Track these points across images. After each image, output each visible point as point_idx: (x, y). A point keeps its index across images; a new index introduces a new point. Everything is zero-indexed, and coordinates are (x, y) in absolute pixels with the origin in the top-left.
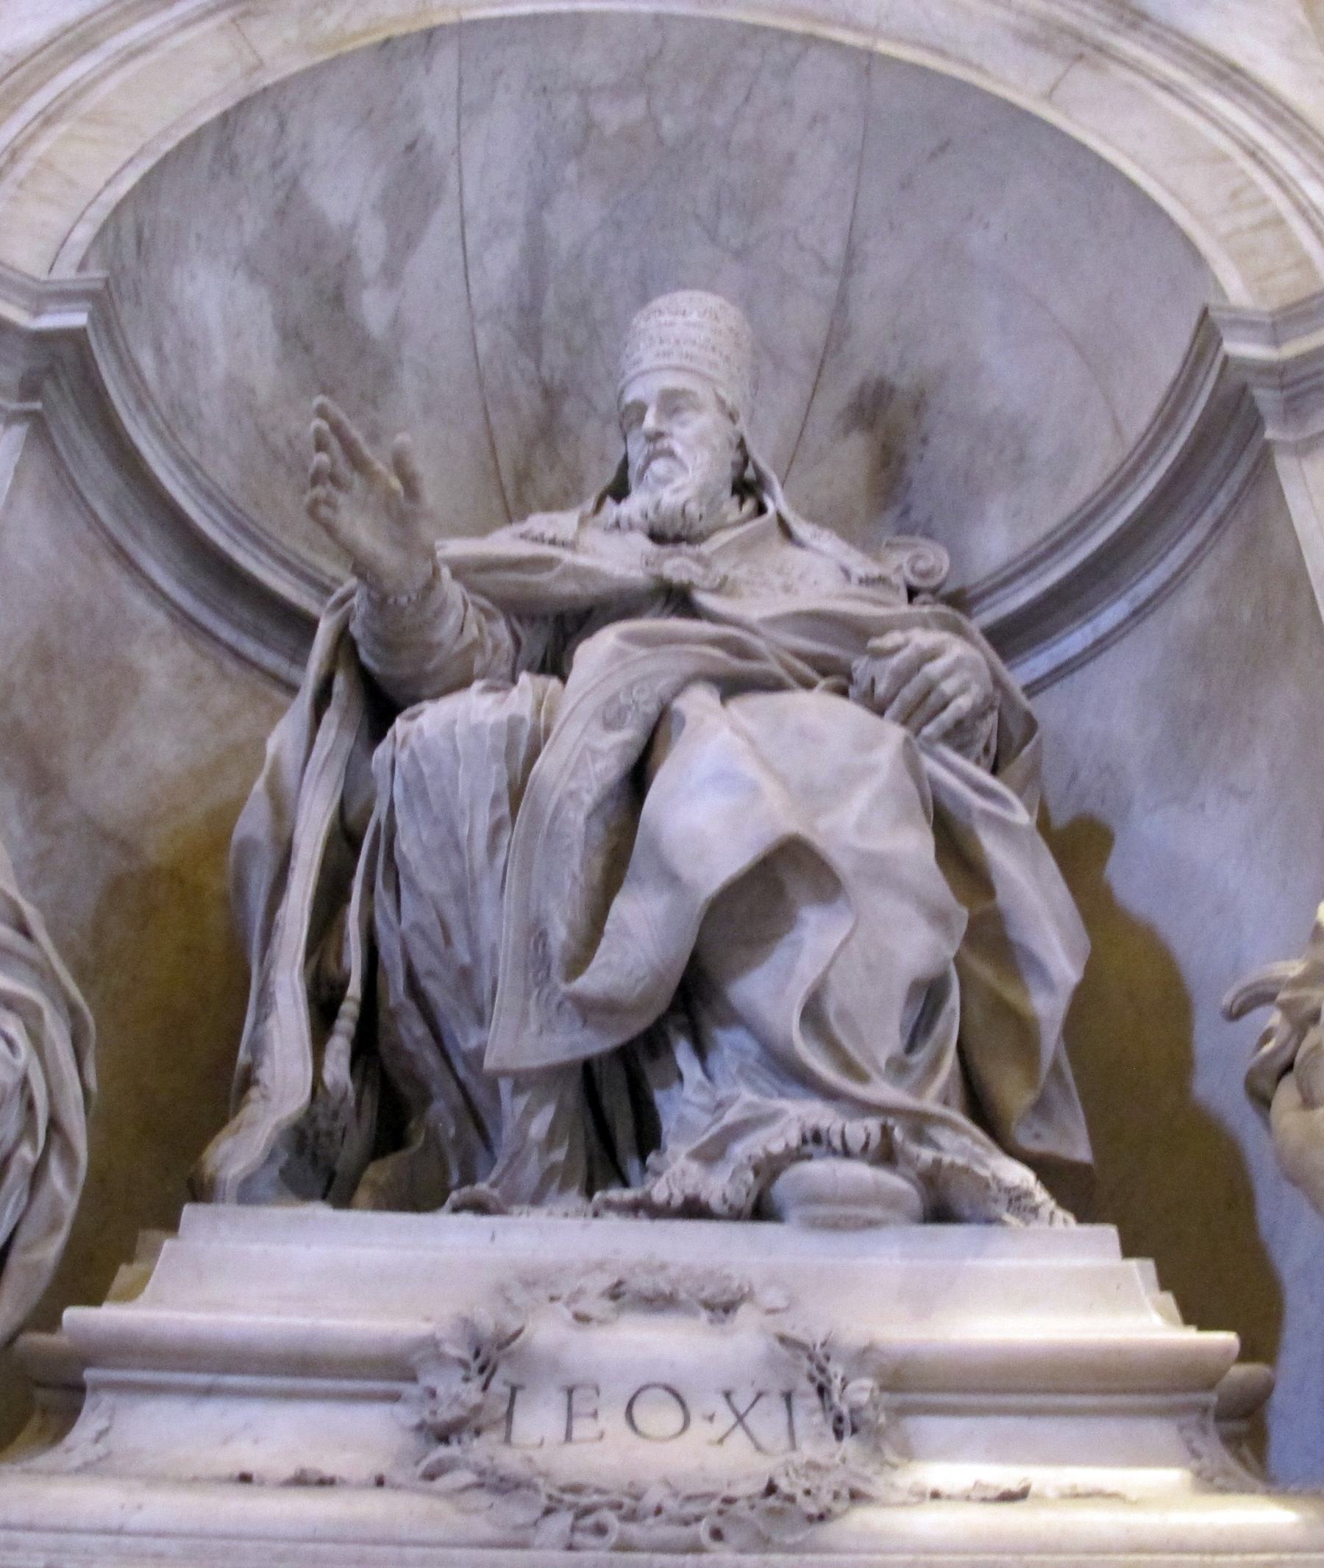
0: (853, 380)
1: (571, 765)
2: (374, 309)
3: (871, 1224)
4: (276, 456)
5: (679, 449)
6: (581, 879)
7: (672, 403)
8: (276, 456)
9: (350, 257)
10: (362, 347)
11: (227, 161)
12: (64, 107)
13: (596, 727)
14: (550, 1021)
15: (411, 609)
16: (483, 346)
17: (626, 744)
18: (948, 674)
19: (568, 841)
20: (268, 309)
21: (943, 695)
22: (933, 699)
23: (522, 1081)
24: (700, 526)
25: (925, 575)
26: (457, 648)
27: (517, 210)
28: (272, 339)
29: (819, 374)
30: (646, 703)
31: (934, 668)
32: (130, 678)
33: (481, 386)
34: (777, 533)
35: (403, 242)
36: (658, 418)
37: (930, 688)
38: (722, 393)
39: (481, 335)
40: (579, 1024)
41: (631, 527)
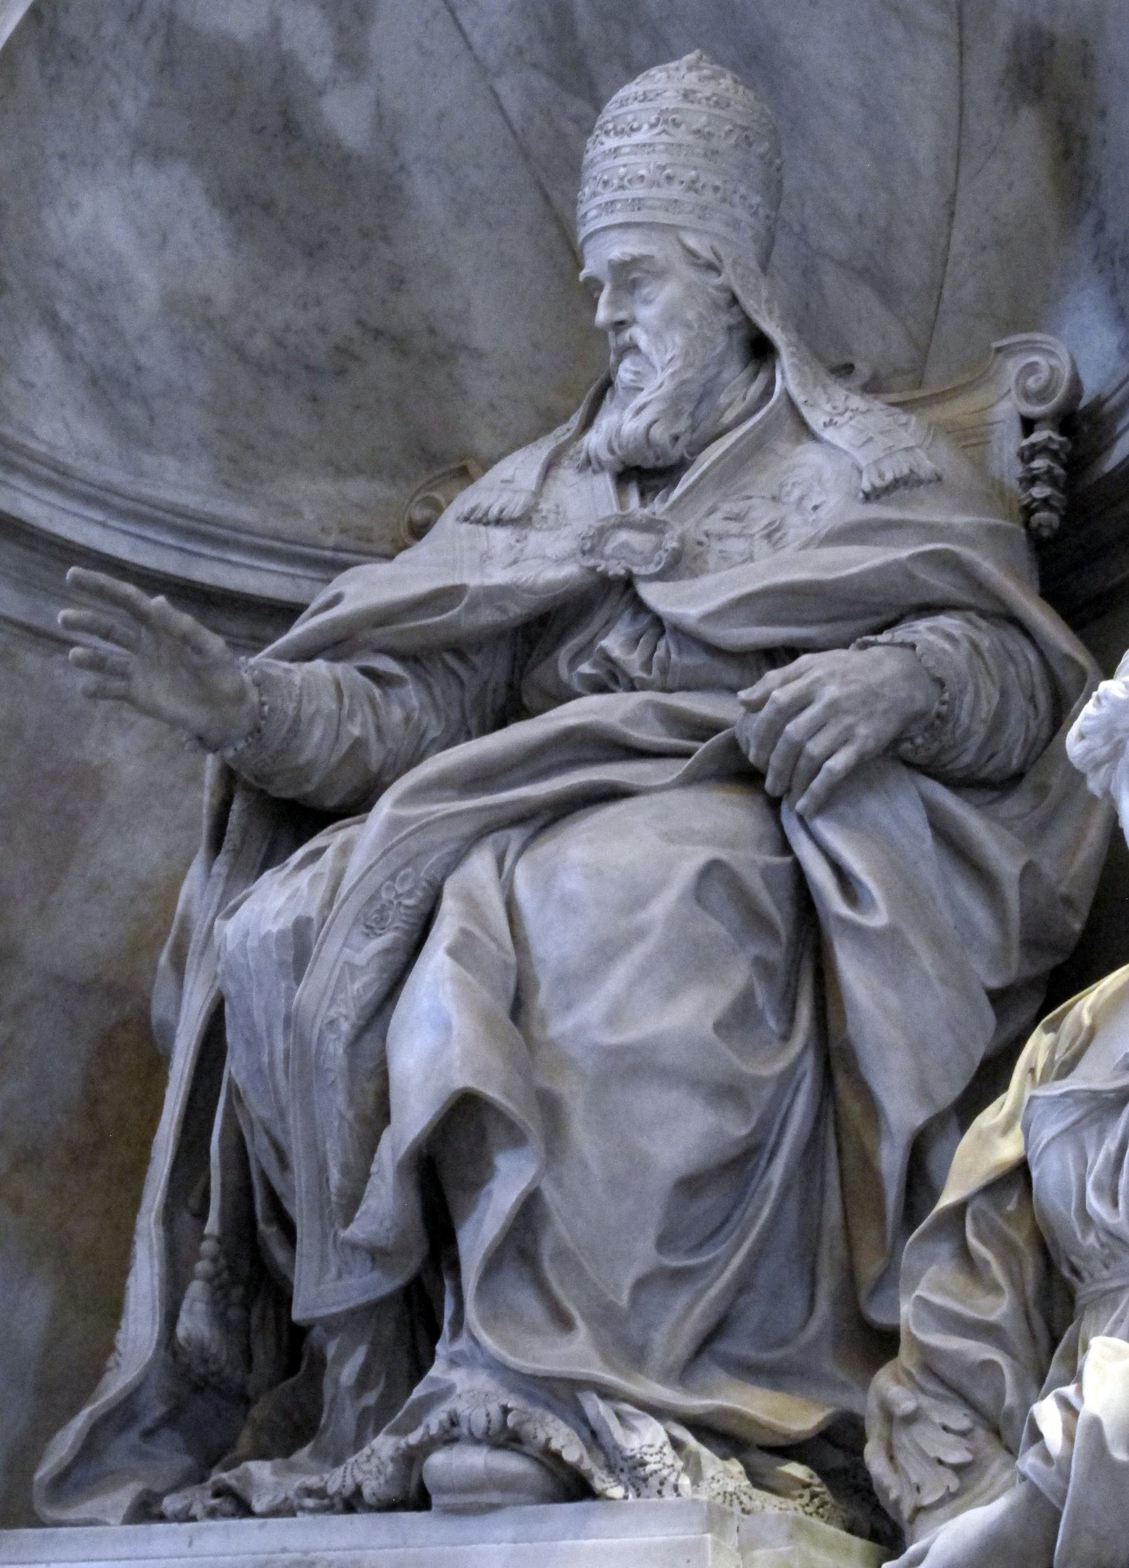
0: (1004, 31)
1: (330, 993)
2: (345, 116)
3: (493, 1508)
4: (261, 369)
5: (643, 341)
6: (350, 1115)
7: (629, 276)
8: (261, 369)
9: (286, 66)
13: (357, 938)
14: (346, 1263)
15: (249, 753)
16: (514, 105)
17: (387, 951)
18: (817, 728)
19: (331, 1077)
21: (811, 758)
22: (803, 763)
23: (333, 1325)
24: (677, 452)
25: (1041, 396)
26: (334, 759)
28: (213, 221)
29: (961, 26)
30: (410, 894)
31: (794, 728)
32: (89, 780)
33: (527, 155)
34: (789, 426)
36: (614, 303)
37: (797, 750)
38: (691, 242)
39: (503, 86)
40: (369, 1264)
41: (601, 467)
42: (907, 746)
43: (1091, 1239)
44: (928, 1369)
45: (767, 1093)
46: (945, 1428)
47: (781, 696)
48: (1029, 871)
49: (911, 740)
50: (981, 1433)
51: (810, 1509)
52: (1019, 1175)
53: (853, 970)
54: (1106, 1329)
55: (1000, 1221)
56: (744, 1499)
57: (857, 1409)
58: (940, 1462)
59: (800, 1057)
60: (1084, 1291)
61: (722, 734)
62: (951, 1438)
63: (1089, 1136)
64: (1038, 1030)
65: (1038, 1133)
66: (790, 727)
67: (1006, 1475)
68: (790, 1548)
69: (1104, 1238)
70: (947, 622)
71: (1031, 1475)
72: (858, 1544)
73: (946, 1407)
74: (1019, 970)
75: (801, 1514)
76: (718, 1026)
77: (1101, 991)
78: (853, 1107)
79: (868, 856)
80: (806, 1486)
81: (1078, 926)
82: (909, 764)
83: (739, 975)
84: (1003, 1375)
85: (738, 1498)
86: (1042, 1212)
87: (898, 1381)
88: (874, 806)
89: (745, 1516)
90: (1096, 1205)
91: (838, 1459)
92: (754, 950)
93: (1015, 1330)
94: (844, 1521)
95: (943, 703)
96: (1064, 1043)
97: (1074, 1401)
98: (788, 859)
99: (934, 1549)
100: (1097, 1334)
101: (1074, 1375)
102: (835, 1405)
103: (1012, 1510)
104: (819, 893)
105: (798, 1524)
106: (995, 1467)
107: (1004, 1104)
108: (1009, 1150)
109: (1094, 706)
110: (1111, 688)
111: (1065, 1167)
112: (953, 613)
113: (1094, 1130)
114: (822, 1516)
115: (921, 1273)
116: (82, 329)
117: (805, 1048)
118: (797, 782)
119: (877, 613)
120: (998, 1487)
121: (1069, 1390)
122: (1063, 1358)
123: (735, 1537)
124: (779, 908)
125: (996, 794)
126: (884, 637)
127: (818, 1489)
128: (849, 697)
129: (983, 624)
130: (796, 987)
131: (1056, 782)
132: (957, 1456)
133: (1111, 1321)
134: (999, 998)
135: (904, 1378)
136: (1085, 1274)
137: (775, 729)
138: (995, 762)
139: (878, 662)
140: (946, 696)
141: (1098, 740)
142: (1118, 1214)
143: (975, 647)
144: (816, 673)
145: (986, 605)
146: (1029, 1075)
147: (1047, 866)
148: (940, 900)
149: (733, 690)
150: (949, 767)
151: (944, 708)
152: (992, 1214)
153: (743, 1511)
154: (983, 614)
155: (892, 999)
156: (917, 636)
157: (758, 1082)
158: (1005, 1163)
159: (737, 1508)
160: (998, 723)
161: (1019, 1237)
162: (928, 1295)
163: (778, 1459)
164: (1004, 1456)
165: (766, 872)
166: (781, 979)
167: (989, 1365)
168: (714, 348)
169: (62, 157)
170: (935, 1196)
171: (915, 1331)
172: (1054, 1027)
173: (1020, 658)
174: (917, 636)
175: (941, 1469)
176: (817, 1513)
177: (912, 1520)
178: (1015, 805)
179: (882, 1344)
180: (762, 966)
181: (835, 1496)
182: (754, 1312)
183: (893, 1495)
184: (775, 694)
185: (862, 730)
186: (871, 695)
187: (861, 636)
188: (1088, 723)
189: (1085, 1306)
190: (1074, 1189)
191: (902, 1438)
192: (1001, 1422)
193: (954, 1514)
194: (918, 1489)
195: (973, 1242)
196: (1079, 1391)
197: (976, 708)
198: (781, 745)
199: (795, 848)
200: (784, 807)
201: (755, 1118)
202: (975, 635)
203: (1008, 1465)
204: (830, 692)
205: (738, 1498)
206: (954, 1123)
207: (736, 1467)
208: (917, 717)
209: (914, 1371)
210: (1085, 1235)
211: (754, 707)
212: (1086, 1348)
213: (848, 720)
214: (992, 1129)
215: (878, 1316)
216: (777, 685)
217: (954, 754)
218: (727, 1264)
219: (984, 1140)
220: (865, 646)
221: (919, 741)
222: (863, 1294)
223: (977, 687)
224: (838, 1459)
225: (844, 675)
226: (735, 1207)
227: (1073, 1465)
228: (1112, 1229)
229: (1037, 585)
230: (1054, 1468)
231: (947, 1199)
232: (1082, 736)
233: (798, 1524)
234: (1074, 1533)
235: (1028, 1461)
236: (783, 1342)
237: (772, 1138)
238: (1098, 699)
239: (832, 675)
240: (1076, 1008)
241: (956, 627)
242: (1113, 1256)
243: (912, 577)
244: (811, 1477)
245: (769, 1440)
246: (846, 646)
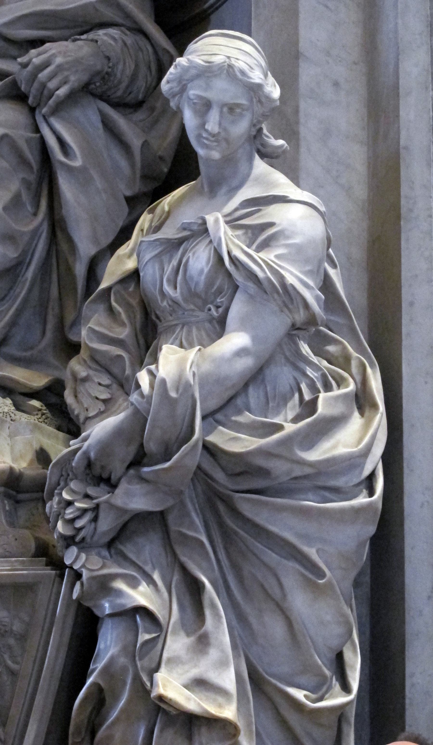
21: (50, 90)
22: (46, 92)
31: (43, 75)
37: (43, 86)
42: (93, 86)
43: (165, 303)
44: (93, 359)
45: (26, 238)
46: (100, 384)
47: (36, 61)
48: (145, 144)
49: (95, 83)
50: (115, 386)
51: (40, 420)
52: (135, 275)
53: (66, 187)
54: (170, 342)
55: (126, 296)
56: (12, 415)
57: (63, 378)
58: (97, 398)
59: (41, 224)
60: (161, 327)
61: (10, 77)
62: (102, 388)
63: (165, 259)
64: (145, 213)
65: (143, 257)
66: (40, 75)
67: (125, 404)
68: (32, 436)
69: (170, 302)
70: (112, 31)
71: (135, 403)
72: (61, 435)
73: (101, 375)
74: (140, 189)
75: (37, 422)
76: (5, 208)
77: (173, 196)
78: (64, 246)
79: (73, 135)
80: (40, 410)
81: (166, 170)
82: (94, 95)
83: (15, 186)
84: (125, 362)
85: (9, 415)
86: (144, 290)
87: (79, 363)
88: (77, 113)
89: (12, 422)
90: (167, 288)
91: (53, 399)
92: (21, 175)
93: (131, 342)
94: (56, 426)
95: (109, 67)
96: (156, 219)
97: (155, 372)
98: (38, 135)
99: (94, 433)
100: (166, 343)
101: (155, 360)
102: (53, 376)
103: (126, 418)
104: (52, 152)
105: (35, 425)
106: (121, 400)
107: (129, 244)
108: (131, 264)
109: (174, 69)
110: (181, 61)
111: (154, 271)
112: (115, 27)
113: (168, 255)
114: (46, 423)
115: (90, 318)
117: (43, 220)
118: (44, 99)
119: (82, 27)
120: (122, 408)
121: (153, 367)
122: (151, 355)
123: (7, 431)
124: (32, 154)
125: (132, 110)
126: (84, 37)
127: (45, 412)
128: (67, 63)
129: (128, 32)
130: (40, 193)
131: (158, 105)
132: (104, 396)
133: (173, 337)
134: (129, 200)
135: (82, 363)
136: (162, 318)
137: (34, 76)
138: (132, 96)
139: (81, 47)
140: (111, 64)
141: (174, 84)
142: (176, 292)
143: (125, 44)
144: (53, 51)
145: (129, 24)
146: (141, 232)
147: (155, 144)
148: (105, 155)
149: (15, 58)
150: (112, 97)
151: (110, 70)
152: (123, 292)
153: (12, 420)
154: (129, 29)
155: (83, 199)
156: (99, 37)
157: (23, 233)
158: (129, 270)
159: (9, 419)
160: (134, 78)
161: (134, 302)
162: (95, 328)
163: (27, 398)
164: (124, 396)
165: (28, 141)
166: (34, 186)
167: (120, 356)
170: (98, 284)
171: (87, 342)
172: (152, 211)
173: (144, 49)
174: (99, 37)
175: (97, 401)
176: (44, 422)
177: (84, 423)
178: (140, 115)
179: (73, 349)
180: (24, 181)
181: (53, 415)
182: (18, 336)
183: (76, 412)
184: (34, 60)
185: (73, 78)
186: (77, 62)
187: (73, 36)
188: (171, 76)
189: (161, 333)
190: (158, 283)
191: (81, 389)
192: (124, 381)
193: (102, 420)
194: (87, 410)
195: (114, 304)
196: (157, 367)
197: (124, 71)
198: (36, 85)
199: (41, 130)
200: (37, 112)
201: (20, 250)
202: (125, 38)
203: (127, 400)
204: (59, 60)
205: (9, 415)
206: (109, 254)
207: (9, 401)
208: (98, 73)
209: (86, 359)
210: (162, 301)
211: (25, 66)
212: (161, 349)
213: (66, 73)
214: (124, 255)
215: (73, 337)
216: (35, 56)
217: (113, 91)
218: (6, 314)
219: (120, 260)
220: (75, 40)
221: (98, 84)
222: (66, 329)
224: (53, 399)
225: (65, 53)
226: (11, 288)
227: (153, 399)
228: (174, 299)
229: (153, 17)
230: (145, 400)
231: (104, 285)
232: (168, 82)
233: (35, 425)
234: (153, 427)
235: (134, 397)
236: (32, 348)
237: (28, 260)
238: (176, 66)
239: (60, 52)
240: (162, 204)
241: (116, 34)
242: (174, 311)
243: (97, 10)
244: (42, 406)
245: (23, 390)
246: (66, 40)
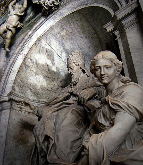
2: (54, 69)
9: (48, 65)
10: (54, 73)
11: (27, 67)
12: (68, 97)
20: (42, 76)
27: (62, 49)
35: (52, 60)
116: (33, 89)
168: (46, 7)
169: (29, 75)
223: (103, 92)
